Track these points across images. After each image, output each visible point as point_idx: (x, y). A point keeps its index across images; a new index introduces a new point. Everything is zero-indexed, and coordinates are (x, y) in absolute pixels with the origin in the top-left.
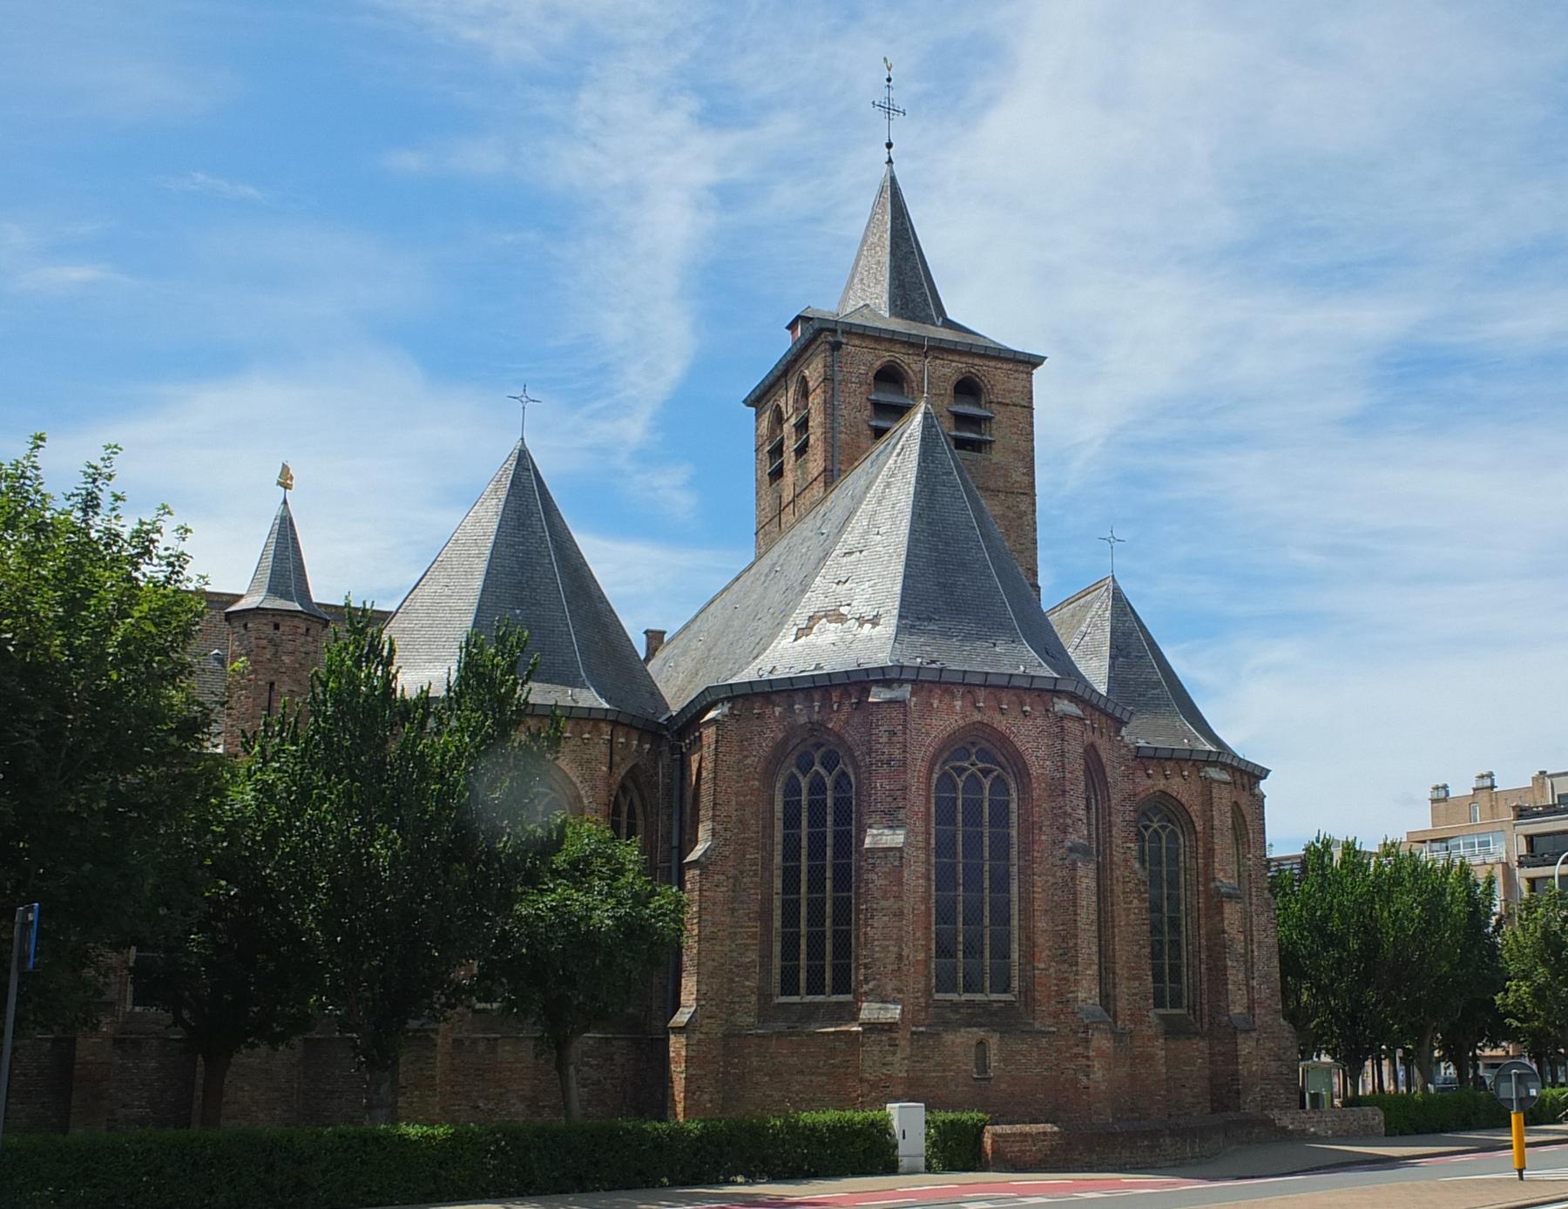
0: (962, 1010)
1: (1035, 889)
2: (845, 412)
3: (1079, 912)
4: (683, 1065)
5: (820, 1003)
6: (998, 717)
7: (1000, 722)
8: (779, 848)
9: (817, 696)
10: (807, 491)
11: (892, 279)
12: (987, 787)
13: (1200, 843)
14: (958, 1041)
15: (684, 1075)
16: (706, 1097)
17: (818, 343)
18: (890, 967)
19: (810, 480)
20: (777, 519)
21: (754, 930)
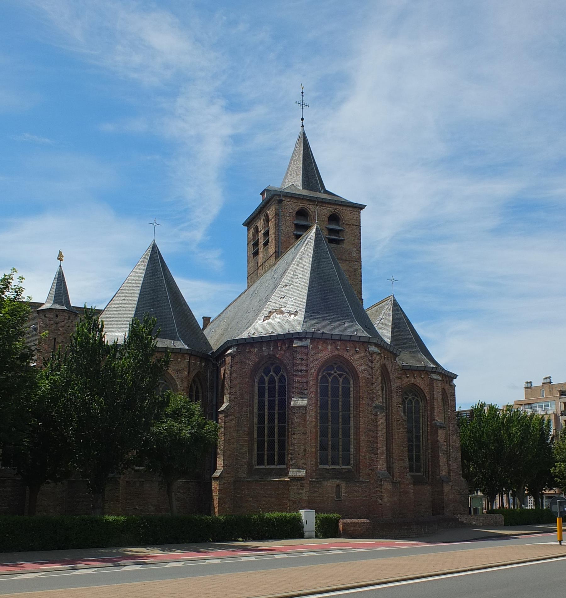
0: (330, 472)
2: (284, 228)
4: (218, 493)
6: (346, 353)
7: (346, 355)
8: (256, 406)
10: (268, 260)
12: (341, 381)
15: (218, 497)
16: (227, 506)
17: (273, 200)
18: (301, 455)
19: (269, 256)
20: (256, 272)
21: (246, 439)
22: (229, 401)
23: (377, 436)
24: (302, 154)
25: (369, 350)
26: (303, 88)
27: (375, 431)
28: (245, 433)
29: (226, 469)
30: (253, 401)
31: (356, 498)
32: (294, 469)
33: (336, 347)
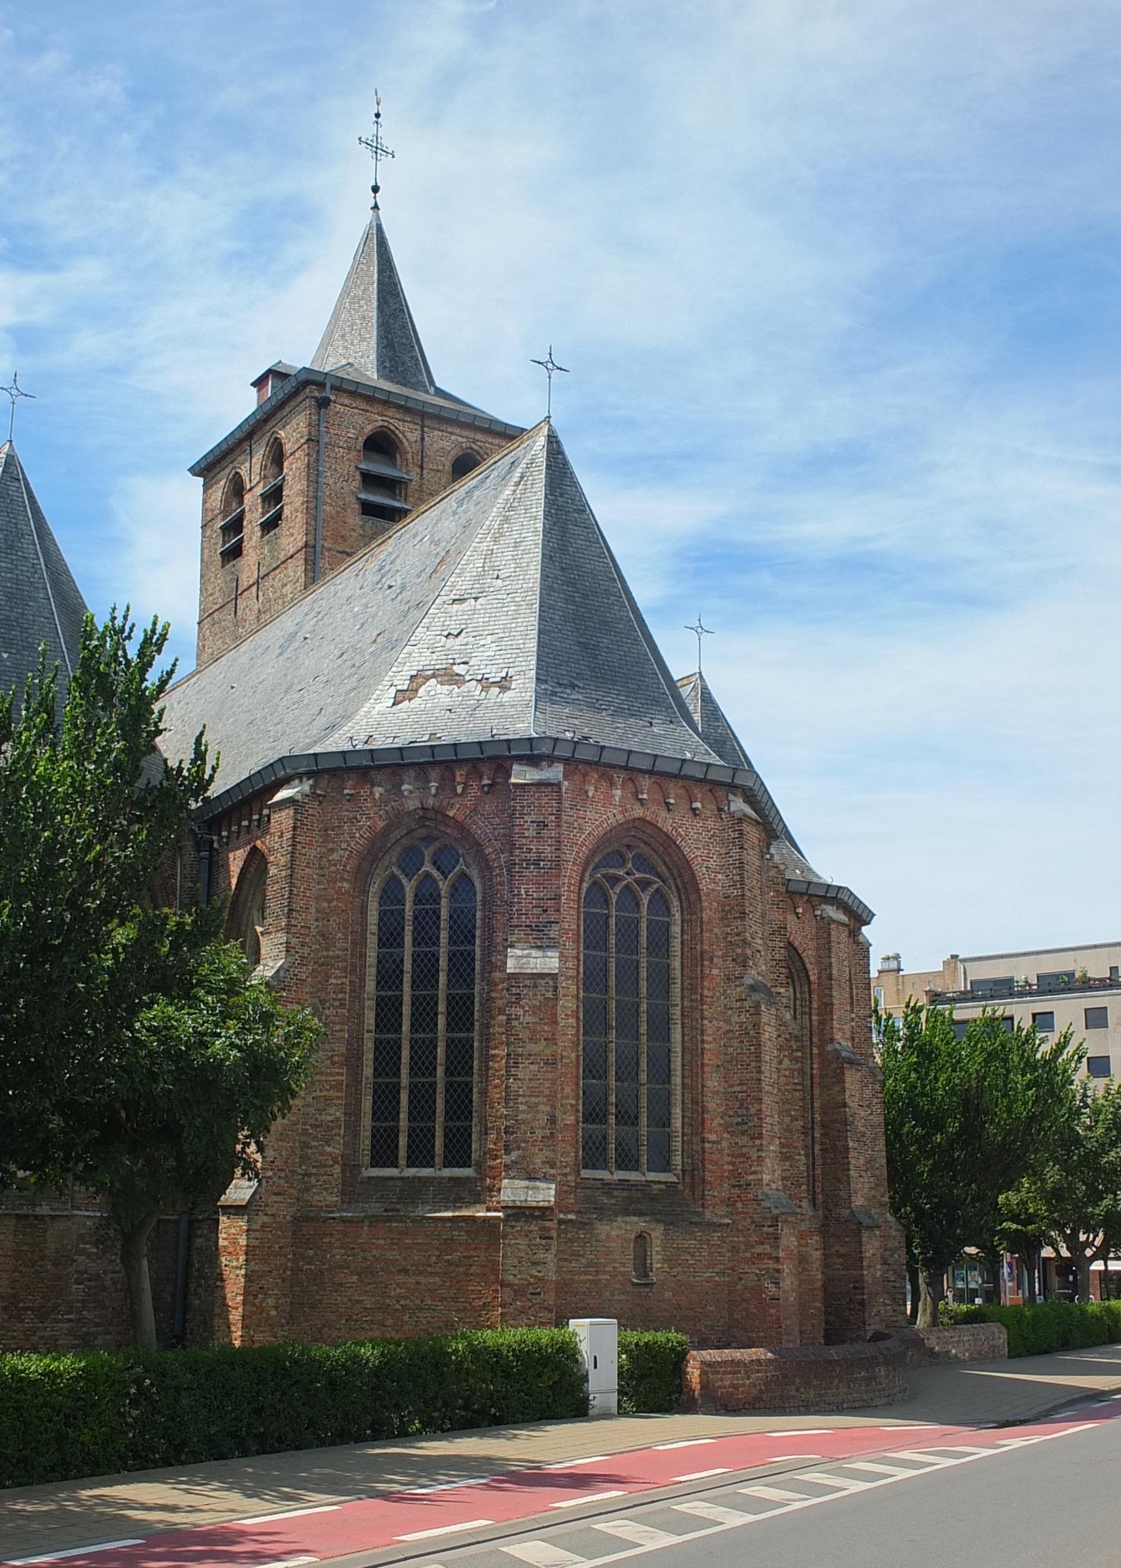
0: (616, 1193)
1: (705, 1038)
2: (331, 481)
3: (763, 1069)
4: (242, 1258)
5: (427, 1178)
6: (663, 814)
7: (666, 822)
8: (371, 973)
9: (434, 774)
10: (278, 571)
11: (380, 337)
12: (646, 902)
13: (815, 997)
14: (614, 1233)
15: (243, 1272)
16: (271, 1301)
17: (301, 398)
18: (539, 1133)
19: (282, 557)
20: (231, 605)
21: (341, 1078)
22: (283, 954)
23: (760, 1080)
24: (376, 281)
25: (732, 809)
26: (378, 104)
27: (753, 1064)
28: (336, 1059)
29: (270, 1177)
30: (363, 956)
31: (691, 1279)
32: (517, 1182)
33: (636, 794)
